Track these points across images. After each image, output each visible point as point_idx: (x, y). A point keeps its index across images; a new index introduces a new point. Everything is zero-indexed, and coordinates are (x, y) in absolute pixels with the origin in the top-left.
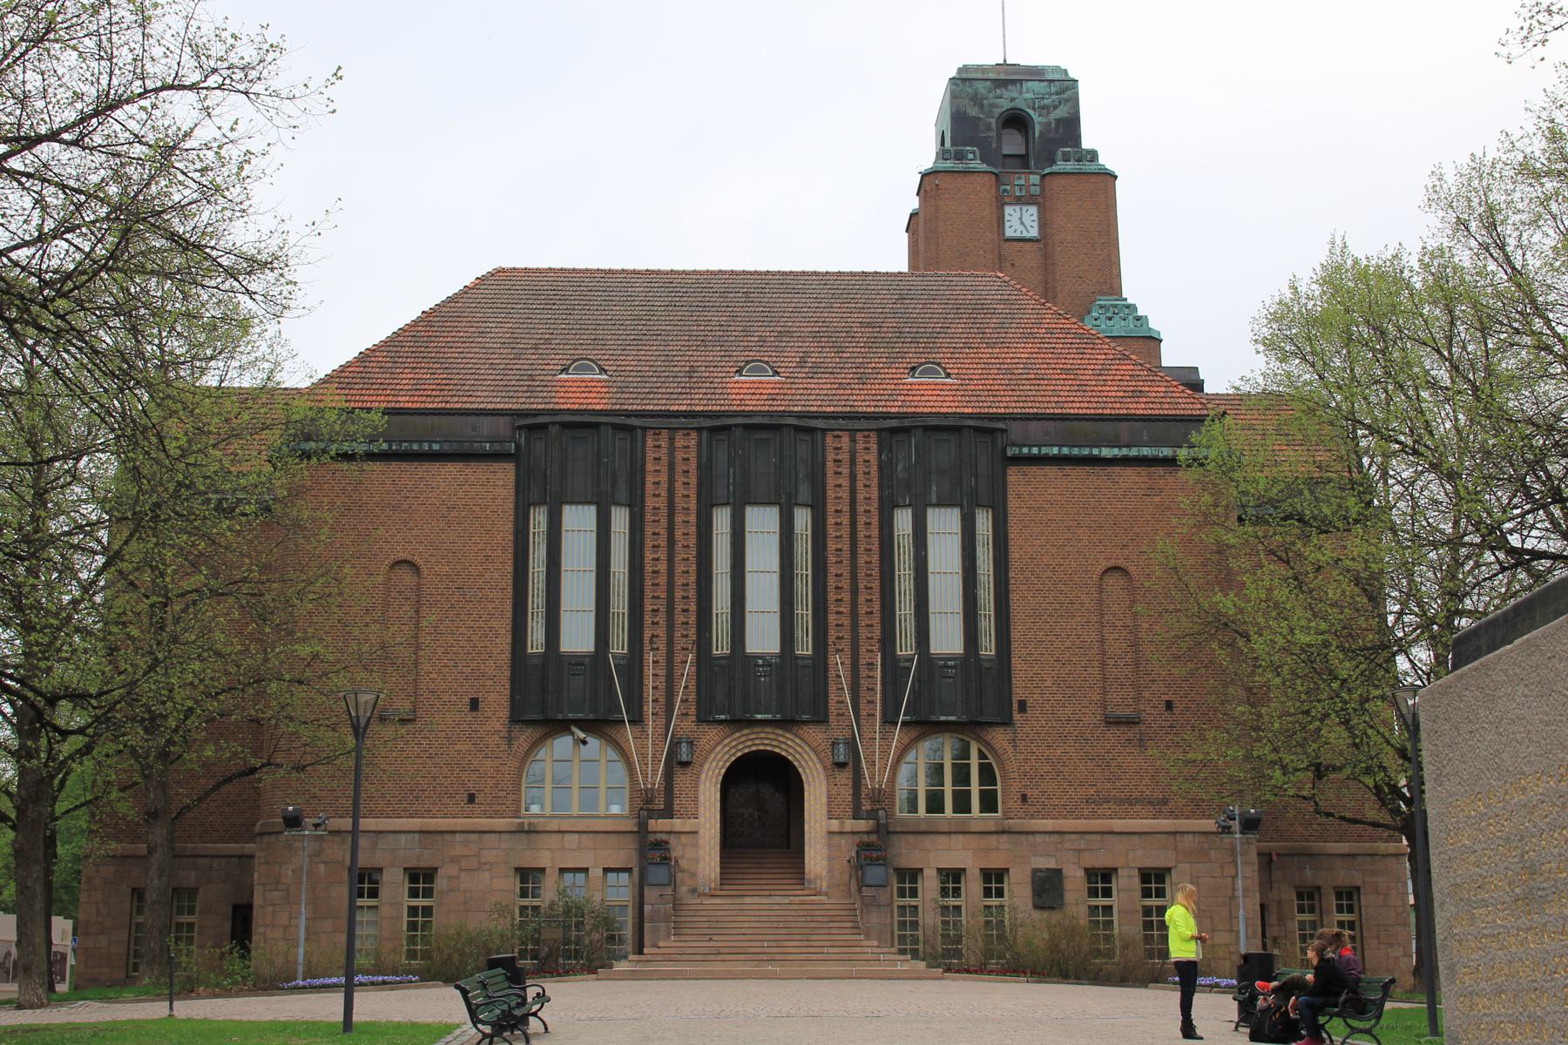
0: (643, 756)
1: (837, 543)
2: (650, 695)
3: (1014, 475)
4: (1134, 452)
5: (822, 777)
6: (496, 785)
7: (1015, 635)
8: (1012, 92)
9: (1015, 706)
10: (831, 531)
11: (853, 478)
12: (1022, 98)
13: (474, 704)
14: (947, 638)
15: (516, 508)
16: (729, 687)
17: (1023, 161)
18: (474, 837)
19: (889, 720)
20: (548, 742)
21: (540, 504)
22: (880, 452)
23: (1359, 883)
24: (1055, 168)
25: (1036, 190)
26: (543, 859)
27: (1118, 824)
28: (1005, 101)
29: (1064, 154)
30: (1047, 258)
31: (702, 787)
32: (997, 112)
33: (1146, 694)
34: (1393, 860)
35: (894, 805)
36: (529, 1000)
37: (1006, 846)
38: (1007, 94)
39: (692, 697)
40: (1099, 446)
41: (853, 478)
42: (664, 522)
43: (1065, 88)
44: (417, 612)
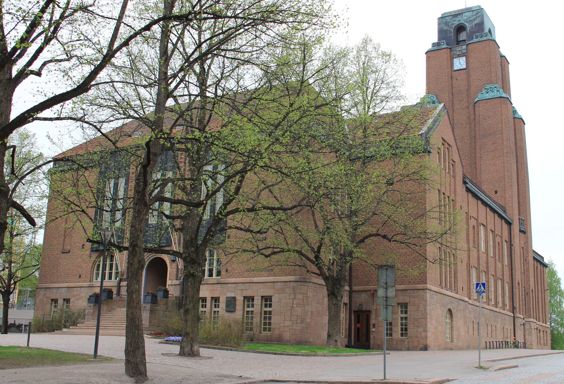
8: (459, 18)
12: (462, 20)
18: (79, 289)
23: (407, 302)
27: (256, 279)
30: (468, 75)
32: (454, 26)
34: (422, 291)
37: (219, 289)
38: (457, 19)
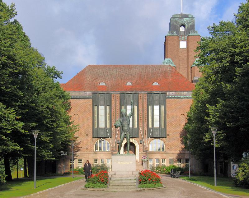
2: (113, 133)
3: (167, 100)
6: (91, 147)
9: (167, 135)
10: (140, 109)
13: (87, 135)
14: (157, 125)
19: (148, 137)
24: (189, 35)
25: (186, 39)
26: (98, 157)
32: (180, 24)
36: (14, 127)
41: (143, 101)
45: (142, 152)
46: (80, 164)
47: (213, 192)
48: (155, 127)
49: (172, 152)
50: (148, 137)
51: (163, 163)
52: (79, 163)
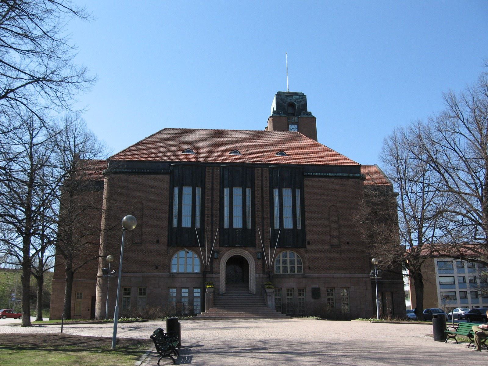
0: (204, 257)
1: (258, 199)
4: (338, 175)
5: (254, 263)
7: (306, 224)
9: (307, 243)
11: (262, 181)
13: (158, 242)
15: (170, 188)
16: (230, 238)
17: (293, 114)
19: (273, 246)
20: (178, 252)
21: (176, 186)
22: (269, 174)
27: (335, 275)
28: (289, 100)
29: (304, 113)
31: (221, 266)
32: (287, 102)
33: (342, 240)
35: (274, 270)
39: (218, 240)
40: (328, 173)
41: (262, 181)
42: (210, 192)
43: (303, 98)
44: (142, 216)
45: (262, 276)
46: (142, 296)
47: (301, 351)
48: (284, 228)
49: (316, 275)
50: (273, 246)
51: (300, 297)
52: (140, 294)
